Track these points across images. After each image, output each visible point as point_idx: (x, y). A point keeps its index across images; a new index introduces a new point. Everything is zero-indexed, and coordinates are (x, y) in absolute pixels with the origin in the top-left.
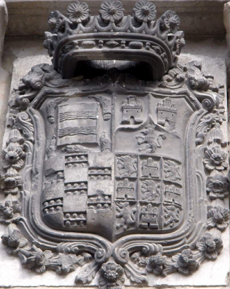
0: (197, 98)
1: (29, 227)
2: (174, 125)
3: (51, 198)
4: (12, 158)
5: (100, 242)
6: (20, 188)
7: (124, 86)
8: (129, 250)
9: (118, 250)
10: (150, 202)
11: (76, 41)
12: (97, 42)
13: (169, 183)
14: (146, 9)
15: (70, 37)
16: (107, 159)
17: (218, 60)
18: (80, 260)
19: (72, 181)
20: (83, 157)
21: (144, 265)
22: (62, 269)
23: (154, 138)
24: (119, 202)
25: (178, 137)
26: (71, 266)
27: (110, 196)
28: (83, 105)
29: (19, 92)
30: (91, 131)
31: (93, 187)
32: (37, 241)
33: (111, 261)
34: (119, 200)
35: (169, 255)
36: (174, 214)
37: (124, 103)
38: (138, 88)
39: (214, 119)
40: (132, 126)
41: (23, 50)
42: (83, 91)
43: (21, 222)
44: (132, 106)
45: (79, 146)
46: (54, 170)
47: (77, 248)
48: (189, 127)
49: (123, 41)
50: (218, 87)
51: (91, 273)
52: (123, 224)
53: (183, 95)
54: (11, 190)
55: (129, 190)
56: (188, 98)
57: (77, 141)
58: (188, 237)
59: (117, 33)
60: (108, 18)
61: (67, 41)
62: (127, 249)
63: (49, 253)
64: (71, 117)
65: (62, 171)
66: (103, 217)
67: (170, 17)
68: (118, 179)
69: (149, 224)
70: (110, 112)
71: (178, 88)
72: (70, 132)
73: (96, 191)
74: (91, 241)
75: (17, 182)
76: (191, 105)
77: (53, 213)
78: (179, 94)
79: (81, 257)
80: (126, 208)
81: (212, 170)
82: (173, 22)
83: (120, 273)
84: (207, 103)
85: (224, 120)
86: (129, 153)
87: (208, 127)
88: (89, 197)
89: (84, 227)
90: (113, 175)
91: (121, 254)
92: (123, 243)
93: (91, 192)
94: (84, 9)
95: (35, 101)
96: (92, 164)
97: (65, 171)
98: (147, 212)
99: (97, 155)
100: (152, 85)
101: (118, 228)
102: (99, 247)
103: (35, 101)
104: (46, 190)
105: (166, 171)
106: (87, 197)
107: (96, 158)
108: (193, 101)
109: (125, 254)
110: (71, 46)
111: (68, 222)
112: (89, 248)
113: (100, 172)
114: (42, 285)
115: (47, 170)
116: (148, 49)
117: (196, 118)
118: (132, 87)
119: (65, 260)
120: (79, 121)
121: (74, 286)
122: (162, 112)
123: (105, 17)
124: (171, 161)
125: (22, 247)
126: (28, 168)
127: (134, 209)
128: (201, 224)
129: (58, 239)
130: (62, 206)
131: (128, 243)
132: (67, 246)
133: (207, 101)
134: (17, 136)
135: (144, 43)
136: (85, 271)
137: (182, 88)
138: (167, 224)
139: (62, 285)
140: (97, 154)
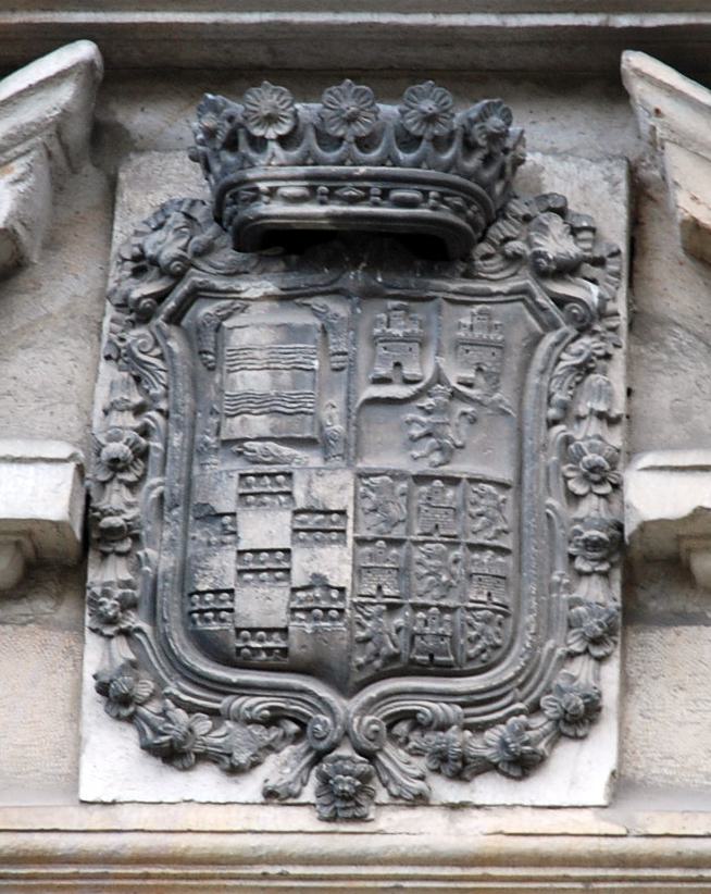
0: (553, 300)
1: (157, 653)
2: (498, 381)
3: (206, 587)
4: (115, 461)
5: (320, 699)
6: (136, 538)
7: (380, 279)
8: (385, 719)
9: (360, 722)
10: (434, 603)
11: (263, 186)
12: (313, 189)
13: (482, 548)
14: (430, 112)
15: (251, 175)
16: (334, 488)
17: (608, 169)
18: (273, 740)
19: (254, 547)
20: (281, 478)
21: (417, 753)
22: (232, 765)
23: (448, 424)
24: (363, 605)
25: (505, 413)
26: (253, 756)
27: (342, 590)
28: (282, 328)
29: (130, 265)
30: (300, 407)
31: (303, 565)
32: (176, 692)
33: (346, 751)
34: (364, 600)
35: (479, 729)
36: (490, 630)
37: (379, 324)
38: (412, 282)
39: (594, 354)
40: (397, 391)
41: (142, 110)
42: (283, 289)
43: (138, 635)
44: (398, 336)
45: (271, 445)
46: (213, 509)
47: (267, 712)
48: (533, 379)
49: (376, 188)
50: (605, 254)
51: (300, 772)
52: (372, 658)
53: (520, 296)
54: (115, 544)
55: (387, 571)
56: (530, 301)
57: (268, 433)
58: (521, 687)
59: (362, 170)
60: (340, 133)
61: (245, 181)
62: (381, 716)
63: (204, 719)
64: (254, 361)
65: (233, 514)
66: (326, 642)
67: (487, 117)
68: (360, 542)
69: (431, 656)
70: (346, 350)
71: (507, 277)
72: (252, 405)
73: (311, 577)
74: (299, 696)
75: (129, 526)
76: (538, 319)
77: (212, 628)
78: (511, 293)
79: (275, 733)
80: (381, 620)
81: (583, 496)
82: (495, 130)
83: (365, 778)
84: (575, 314)
85: (617, 346)
86: (388, 470)
87: (579, 375)
88: (294, 590)
89: (286, 662)
90: (350, 533)
91: (369, 732)
92: (372, 702)
93: (298, 579)
94: (282, 104)
95: (171, 304)
96: (301, 504)
97: (236, 592)
98: (428, 630)
99: (314, 476)
100: (447, 274)
101: (360, 667)
102: (320, 711)
103: (171, 304)
104: (195, 563)
105: (474, 515)
106: (288, 592)
107: (310, 483)
108: (544, 309)
109: (376, 732)
110: (251, 194)
111: (246, 651)
112: (295, 711)
113: (319, 524)
114: (187, 798)
115: (198, 504)
116: (434, 208)
117: (550, 354)
118: (399, 281)
119: (238, 740)
120: (273, 375)
121: (262, 804)
122: (469, 348)
123: (333, 129)
124: (486, 486)
125: (141, 705)
126: (153, 488)
127: (399, 621)
128: (552, 651)
129: (224, 688)
130: (231, 610)
131: (383, 702)
132: (246, 705)
133: (577, 309)
134: (129, 394)
135: (425, 194)
136: (286, 764)
137: (517, 277)
138: (473, 656)
139: (232, 801)
140: (313, 471)
